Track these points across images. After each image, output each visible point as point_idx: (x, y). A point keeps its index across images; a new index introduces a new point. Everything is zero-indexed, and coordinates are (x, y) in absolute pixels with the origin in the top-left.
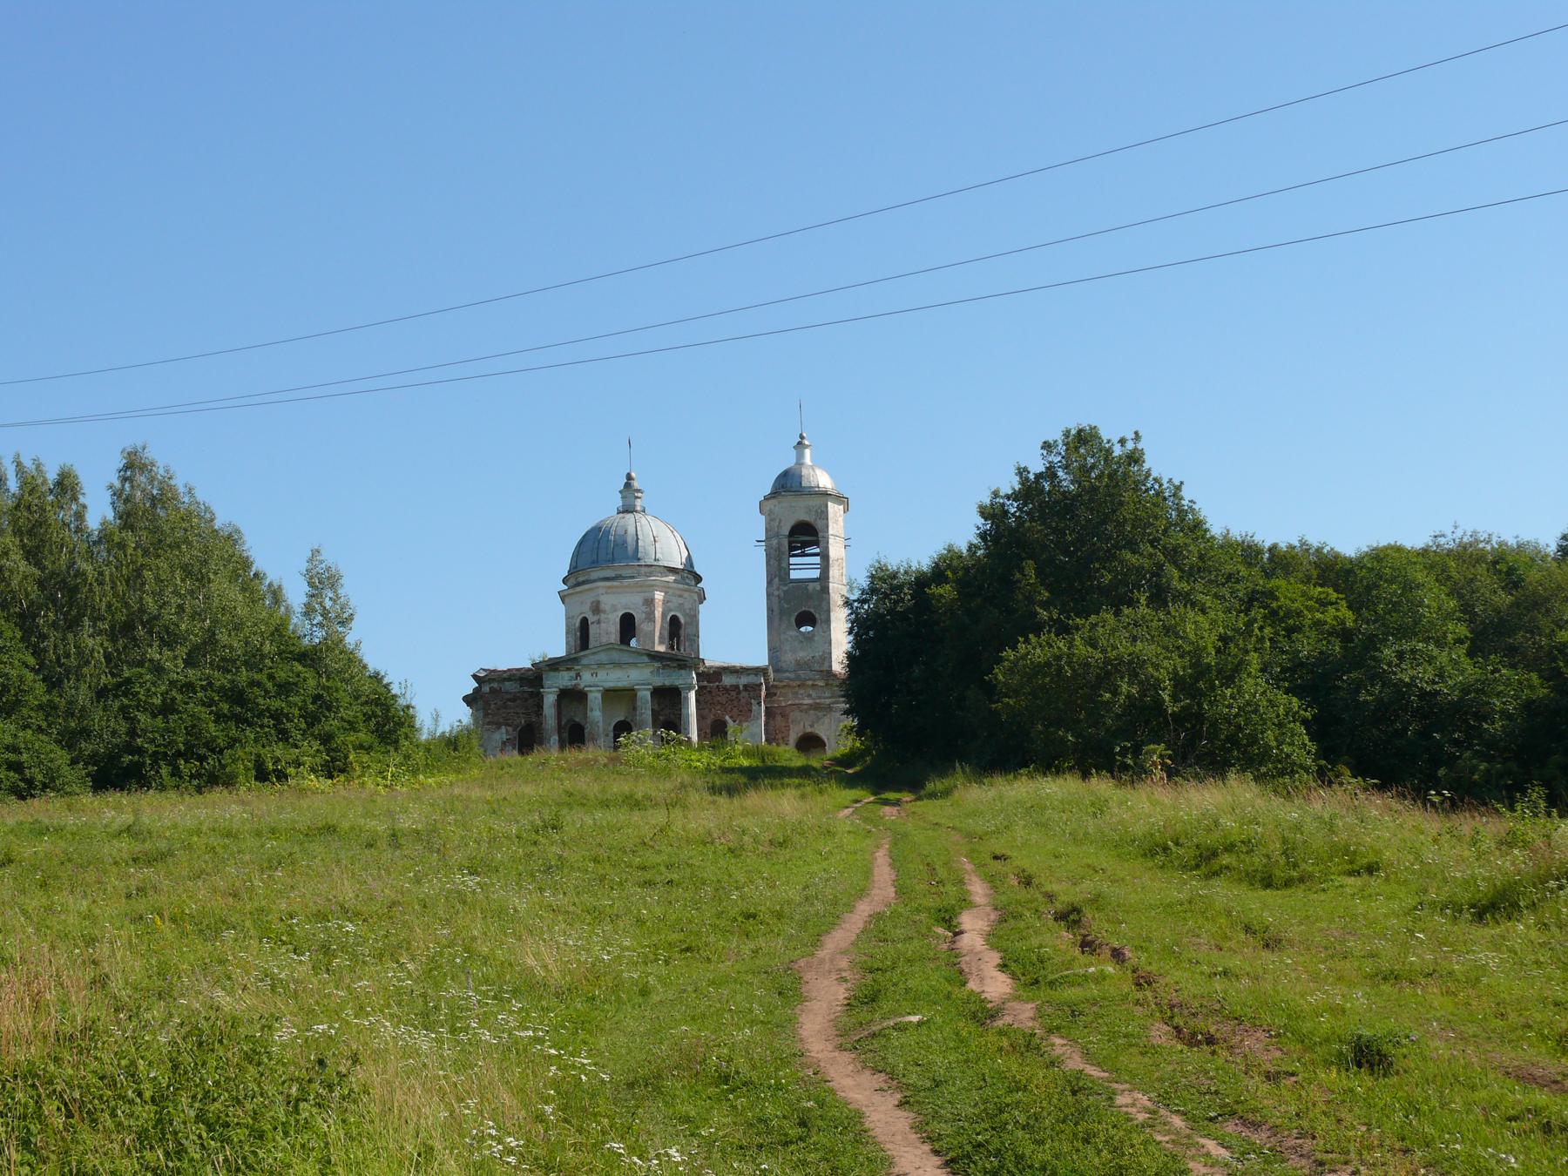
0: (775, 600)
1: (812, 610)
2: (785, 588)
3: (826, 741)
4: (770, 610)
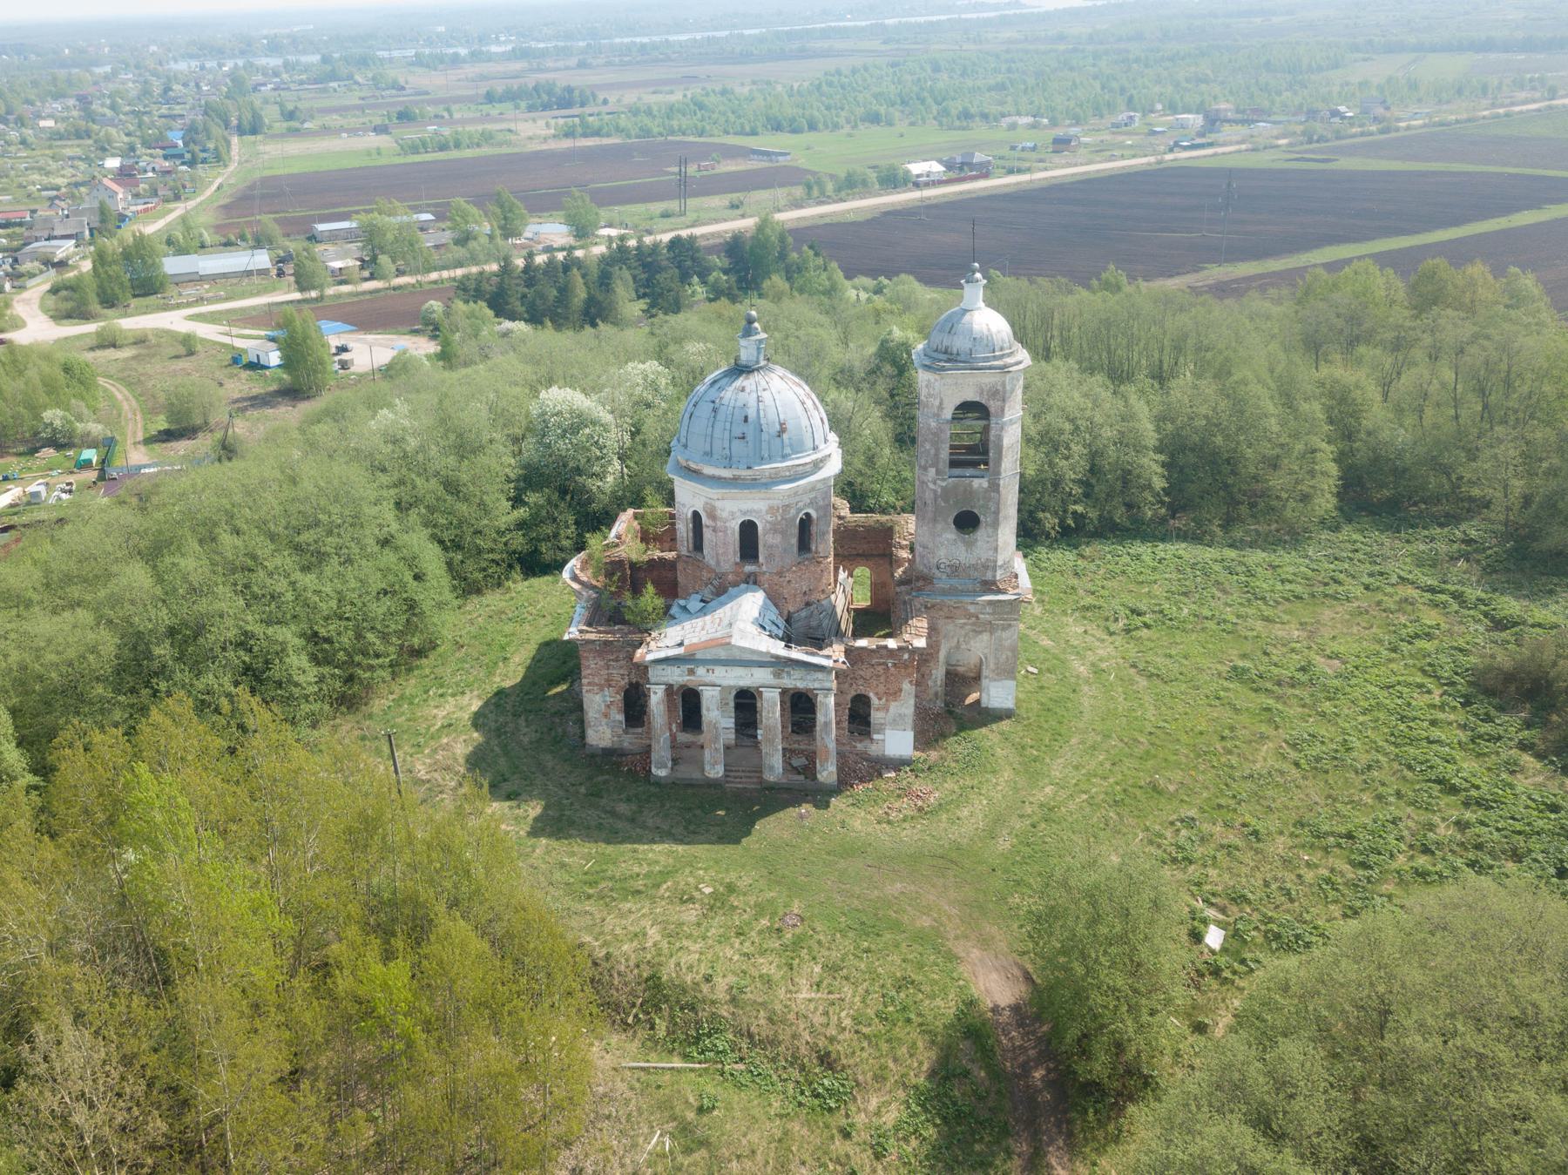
1: (976, 511)
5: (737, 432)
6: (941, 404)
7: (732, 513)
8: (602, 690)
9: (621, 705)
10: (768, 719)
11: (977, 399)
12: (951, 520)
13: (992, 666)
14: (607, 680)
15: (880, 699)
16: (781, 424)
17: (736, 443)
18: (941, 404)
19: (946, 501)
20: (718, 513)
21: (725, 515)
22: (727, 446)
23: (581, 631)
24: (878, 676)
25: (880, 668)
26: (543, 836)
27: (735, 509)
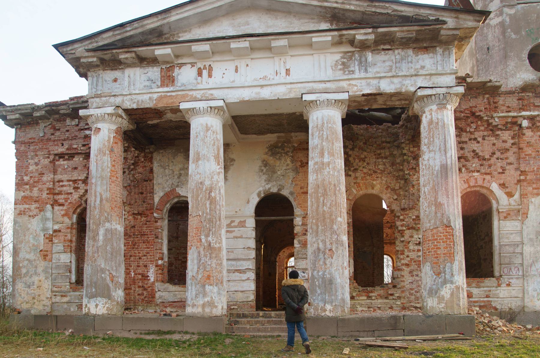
2: (512, 11)
8: (41, 210)
14: (51, 192)
15: (510, 195)
25: (506, 135)
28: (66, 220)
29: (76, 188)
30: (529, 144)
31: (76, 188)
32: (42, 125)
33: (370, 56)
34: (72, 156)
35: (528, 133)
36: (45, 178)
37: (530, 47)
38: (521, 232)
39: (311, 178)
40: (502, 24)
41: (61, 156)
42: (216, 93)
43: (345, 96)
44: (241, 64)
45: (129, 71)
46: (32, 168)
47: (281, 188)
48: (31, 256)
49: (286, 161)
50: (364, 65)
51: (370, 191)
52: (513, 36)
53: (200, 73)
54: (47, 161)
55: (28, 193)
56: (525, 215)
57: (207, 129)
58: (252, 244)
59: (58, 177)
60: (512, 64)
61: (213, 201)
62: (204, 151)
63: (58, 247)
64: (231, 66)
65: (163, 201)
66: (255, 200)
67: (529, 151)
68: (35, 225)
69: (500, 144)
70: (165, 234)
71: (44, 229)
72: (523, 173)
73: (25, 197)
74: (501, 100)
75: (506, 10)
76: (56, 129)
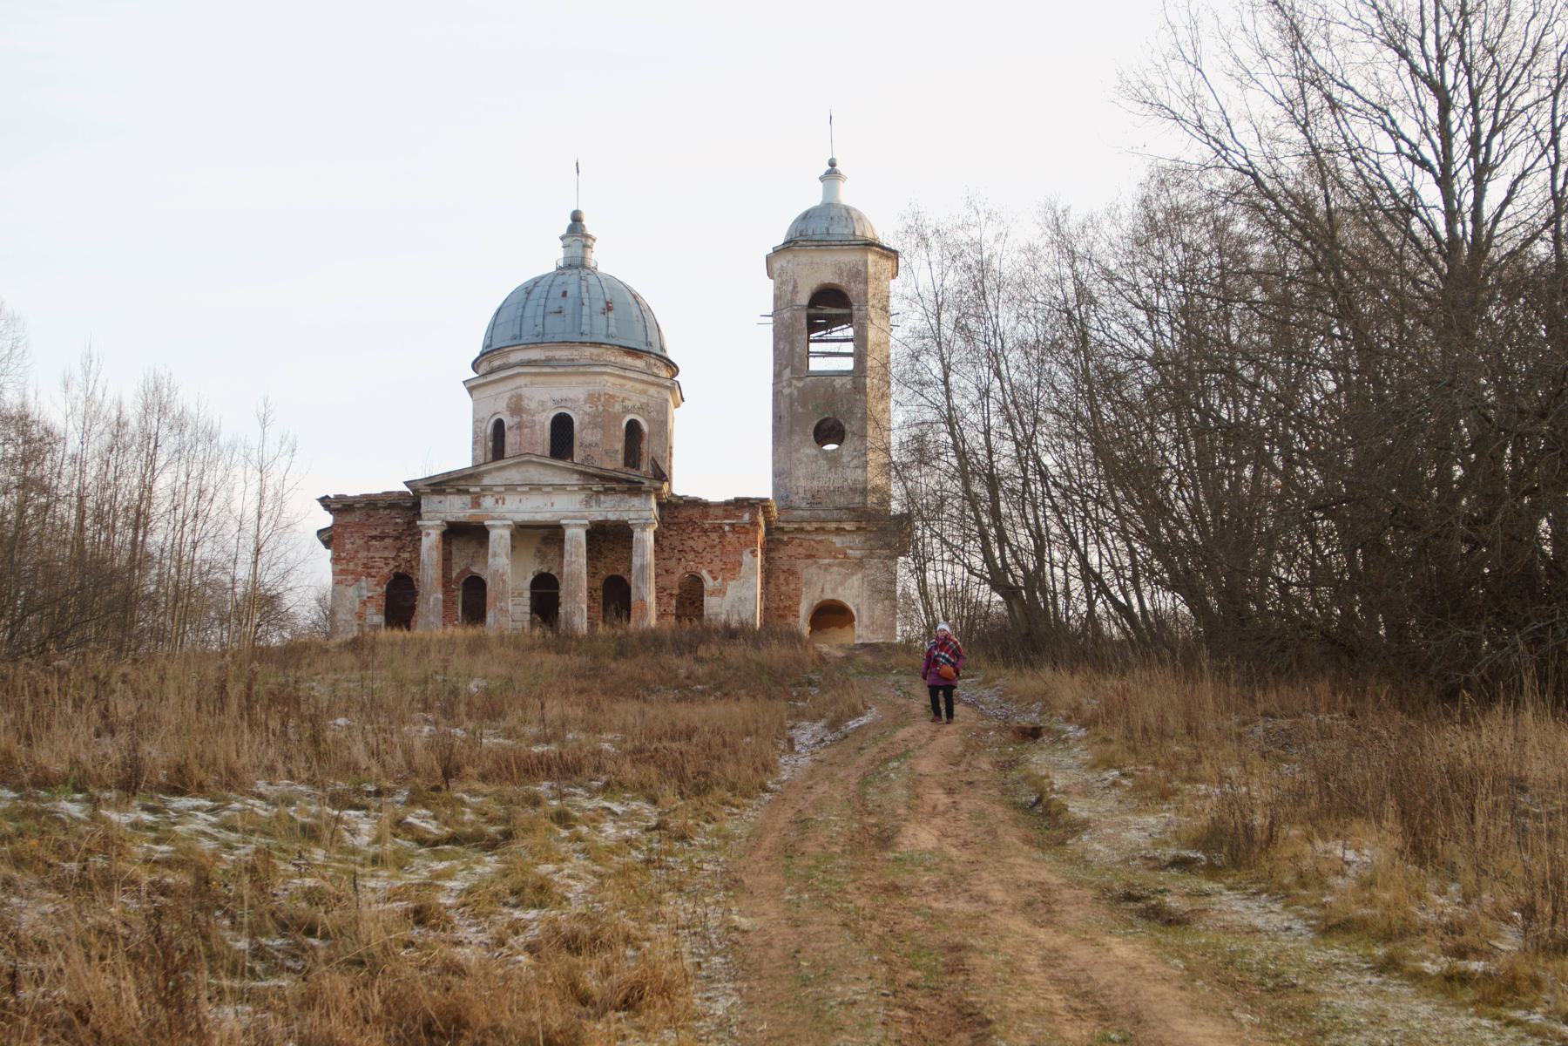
0: (784, 404)
2: (801, 384)
3: (855, 613)
4: (777, 418)
5: (553, 307)
6: (795, 287)
7: (542, 403)
8: (357, 580)
9: (382, 602)
10: (571, 563)
11: (836, 281)
12: (811, 430)
13: (866, 620)
14: (365, 566)
15: (715, 578)
16: (607, 303)
17: (550, 319)
18: (795, 287)
19: (804, 406)
20: (525, 403)
21: (533, 405)
22: (539, 321)
23: (288, 785)
24: (713, 547)
25: (714, 536)
26: (280, 648)
27: (546, 398)
28: (378, 589)
29: (387, 564)
30: (730, 543)
31: (387, 564)
32: (358, 513)
33: (602, 497)
34: (382, 538)
35: (730, 535)
36: (360, 555)
37: (816, 422)
38: (720, 606)
39: (565, 569)
40: (791, 395)
41: (374, 538)
42: (507, 515)
43: (586, 522)
44: (524, 497)
45: (449, 497)
46: (349, 546)
47: (551, 569)
48: (348, 617)
49: (405, 1031)
50: (599, 503)
51: (616, 573)
52: (800, 410)
53: (497, 502)
54: (361, 542)
55: (345, 567)
56: (724, 593)
57: (501, 537)
58: (528, 609)
59: (372, 554)
60: (797, 439)
61: (504, 582)
62: (499, 551)
63: (371, 609)
64: (517, 498)
65: (459, 576)
66: (530, 578)
67: (729, 548)
68: (351, 592)
69: (709, 542)
70: (460, 601)
71: (359, 596)
72: (725, 563)
73: (342, 570)
74: (711, 511)
75: (795, 382)
76: (370, 516)
